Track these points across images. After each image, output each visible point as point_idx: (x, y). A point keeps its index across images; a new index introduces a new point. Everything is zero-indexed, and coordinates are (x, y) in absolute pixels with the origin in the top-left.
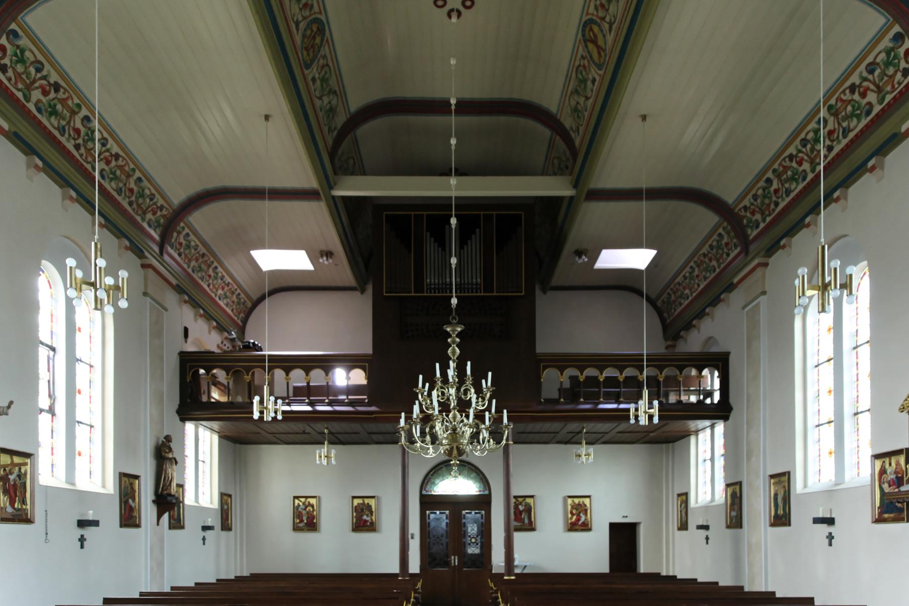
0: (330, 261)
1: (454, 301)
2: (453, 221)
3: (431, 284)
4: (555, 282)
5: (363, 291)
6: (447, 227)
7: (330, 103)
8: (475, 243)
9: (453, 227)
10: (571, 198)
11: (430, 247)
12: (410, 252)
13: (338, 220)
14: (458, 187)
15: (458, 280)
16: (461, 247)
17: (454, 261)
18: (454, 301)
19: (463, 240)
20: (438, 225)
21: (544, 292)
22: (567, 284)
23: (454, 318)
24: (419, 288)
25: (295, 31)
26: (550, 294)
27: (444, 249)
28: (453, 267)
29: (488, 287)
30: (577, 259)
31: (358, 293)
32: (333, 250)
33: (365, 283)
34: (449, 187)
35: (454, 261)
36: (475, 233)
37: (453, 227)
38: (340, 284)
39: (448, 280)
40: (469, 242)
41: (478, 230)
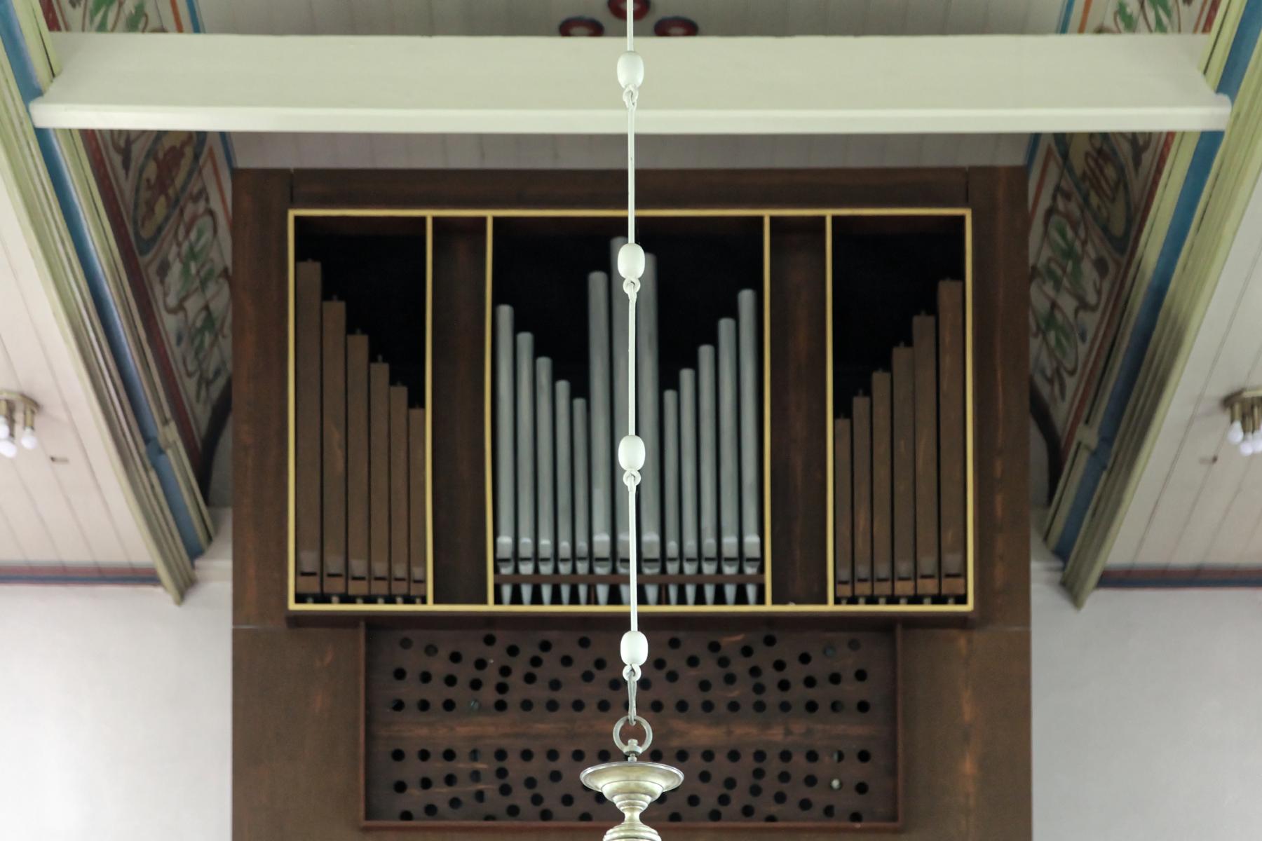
0: (27, 440)
1: (634, 649)
2: (632, 263)
3: (516, 558)
4: (1121, 549)
5: (185, 586)
6: (597, 280)
7: (206, 308)
8: (737, 351)
9: (631, 291)
10: (1209, 142)
11: (512, 365)
12: (416, 400)
13: (65, 250)
14: (648, 96)
15: (651, 537)
16: (667, 380)
17: (633, 454)
18: (634, 649)
19: (681, 333)
20: (549, 272)
21: (1071, 588)
22: (1185, 557)
23: (633, 732)
24: (459, 575)
25: (121, 172)
26: (1100, 601)
27: (581, 389)
28: (630, 482)
29: (798, 574)
30: (1236, 432)
31: (160, 598)
32: (40, 387)
33: (195, 552)
34: (612, 96)
35: (633, 454)
36: (733, 312)
37: (631, 291)
38: (74, 554)
39: (602, 538)
40: (705, 352)
41: (746, 298)
